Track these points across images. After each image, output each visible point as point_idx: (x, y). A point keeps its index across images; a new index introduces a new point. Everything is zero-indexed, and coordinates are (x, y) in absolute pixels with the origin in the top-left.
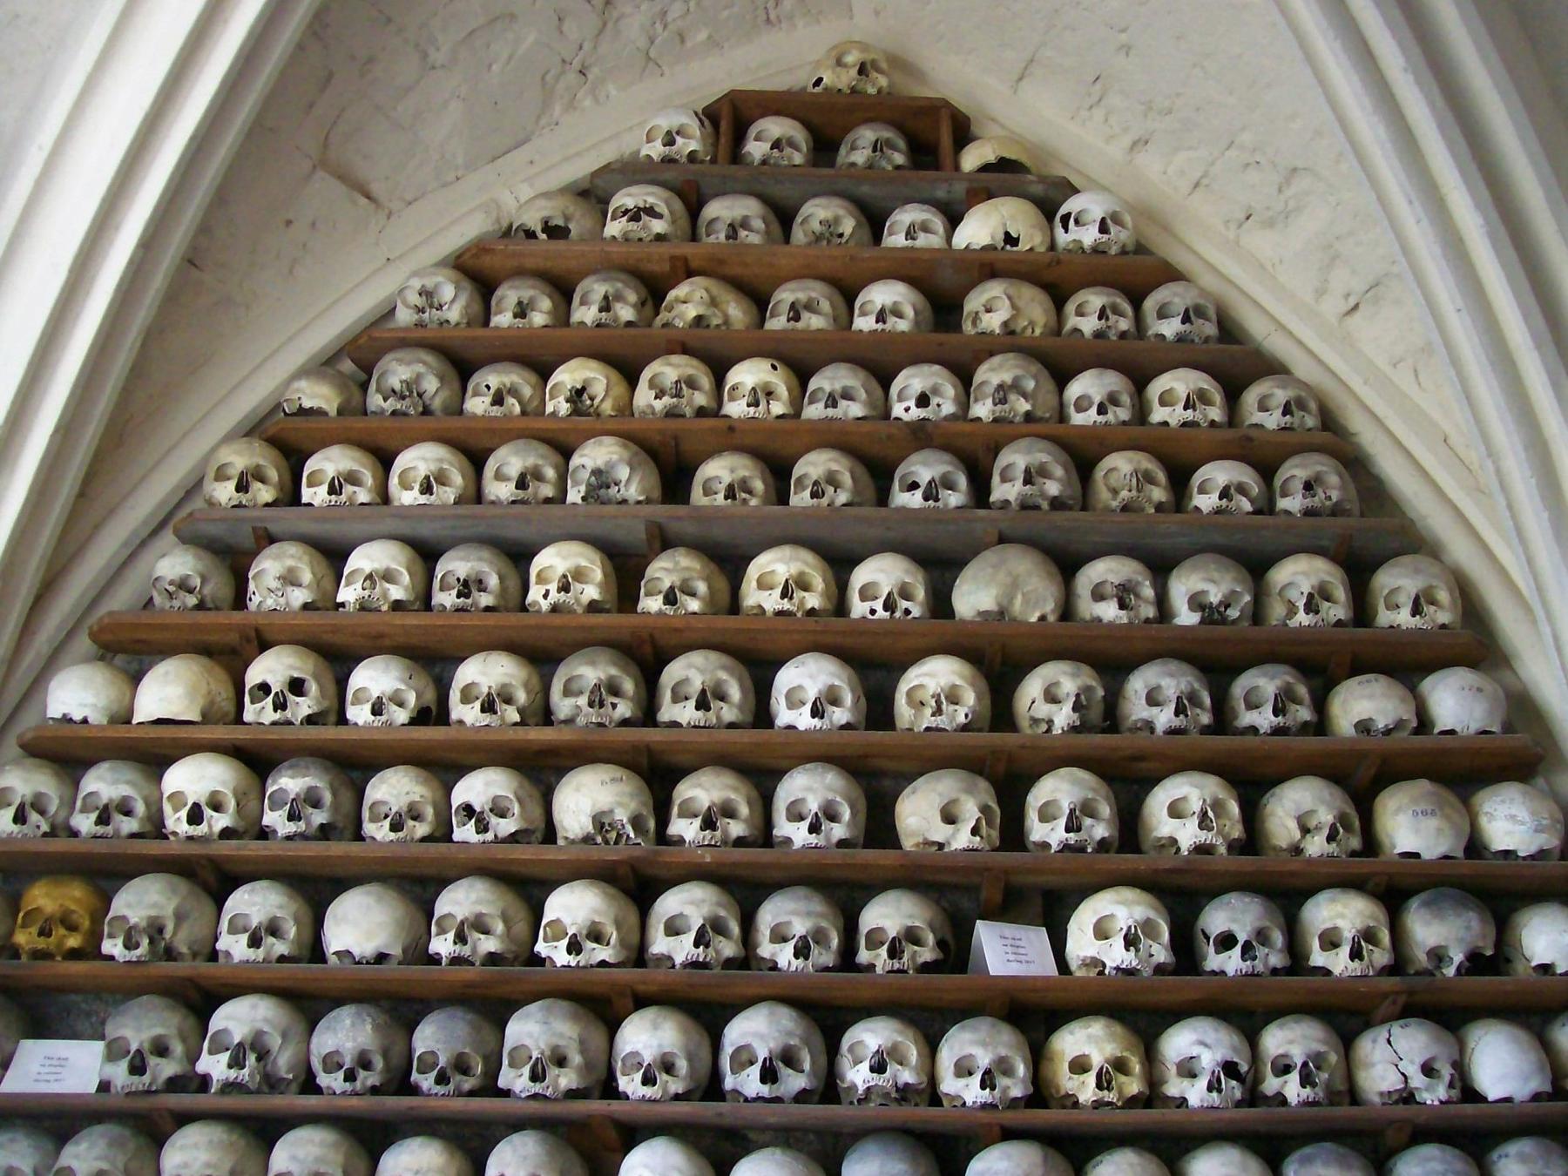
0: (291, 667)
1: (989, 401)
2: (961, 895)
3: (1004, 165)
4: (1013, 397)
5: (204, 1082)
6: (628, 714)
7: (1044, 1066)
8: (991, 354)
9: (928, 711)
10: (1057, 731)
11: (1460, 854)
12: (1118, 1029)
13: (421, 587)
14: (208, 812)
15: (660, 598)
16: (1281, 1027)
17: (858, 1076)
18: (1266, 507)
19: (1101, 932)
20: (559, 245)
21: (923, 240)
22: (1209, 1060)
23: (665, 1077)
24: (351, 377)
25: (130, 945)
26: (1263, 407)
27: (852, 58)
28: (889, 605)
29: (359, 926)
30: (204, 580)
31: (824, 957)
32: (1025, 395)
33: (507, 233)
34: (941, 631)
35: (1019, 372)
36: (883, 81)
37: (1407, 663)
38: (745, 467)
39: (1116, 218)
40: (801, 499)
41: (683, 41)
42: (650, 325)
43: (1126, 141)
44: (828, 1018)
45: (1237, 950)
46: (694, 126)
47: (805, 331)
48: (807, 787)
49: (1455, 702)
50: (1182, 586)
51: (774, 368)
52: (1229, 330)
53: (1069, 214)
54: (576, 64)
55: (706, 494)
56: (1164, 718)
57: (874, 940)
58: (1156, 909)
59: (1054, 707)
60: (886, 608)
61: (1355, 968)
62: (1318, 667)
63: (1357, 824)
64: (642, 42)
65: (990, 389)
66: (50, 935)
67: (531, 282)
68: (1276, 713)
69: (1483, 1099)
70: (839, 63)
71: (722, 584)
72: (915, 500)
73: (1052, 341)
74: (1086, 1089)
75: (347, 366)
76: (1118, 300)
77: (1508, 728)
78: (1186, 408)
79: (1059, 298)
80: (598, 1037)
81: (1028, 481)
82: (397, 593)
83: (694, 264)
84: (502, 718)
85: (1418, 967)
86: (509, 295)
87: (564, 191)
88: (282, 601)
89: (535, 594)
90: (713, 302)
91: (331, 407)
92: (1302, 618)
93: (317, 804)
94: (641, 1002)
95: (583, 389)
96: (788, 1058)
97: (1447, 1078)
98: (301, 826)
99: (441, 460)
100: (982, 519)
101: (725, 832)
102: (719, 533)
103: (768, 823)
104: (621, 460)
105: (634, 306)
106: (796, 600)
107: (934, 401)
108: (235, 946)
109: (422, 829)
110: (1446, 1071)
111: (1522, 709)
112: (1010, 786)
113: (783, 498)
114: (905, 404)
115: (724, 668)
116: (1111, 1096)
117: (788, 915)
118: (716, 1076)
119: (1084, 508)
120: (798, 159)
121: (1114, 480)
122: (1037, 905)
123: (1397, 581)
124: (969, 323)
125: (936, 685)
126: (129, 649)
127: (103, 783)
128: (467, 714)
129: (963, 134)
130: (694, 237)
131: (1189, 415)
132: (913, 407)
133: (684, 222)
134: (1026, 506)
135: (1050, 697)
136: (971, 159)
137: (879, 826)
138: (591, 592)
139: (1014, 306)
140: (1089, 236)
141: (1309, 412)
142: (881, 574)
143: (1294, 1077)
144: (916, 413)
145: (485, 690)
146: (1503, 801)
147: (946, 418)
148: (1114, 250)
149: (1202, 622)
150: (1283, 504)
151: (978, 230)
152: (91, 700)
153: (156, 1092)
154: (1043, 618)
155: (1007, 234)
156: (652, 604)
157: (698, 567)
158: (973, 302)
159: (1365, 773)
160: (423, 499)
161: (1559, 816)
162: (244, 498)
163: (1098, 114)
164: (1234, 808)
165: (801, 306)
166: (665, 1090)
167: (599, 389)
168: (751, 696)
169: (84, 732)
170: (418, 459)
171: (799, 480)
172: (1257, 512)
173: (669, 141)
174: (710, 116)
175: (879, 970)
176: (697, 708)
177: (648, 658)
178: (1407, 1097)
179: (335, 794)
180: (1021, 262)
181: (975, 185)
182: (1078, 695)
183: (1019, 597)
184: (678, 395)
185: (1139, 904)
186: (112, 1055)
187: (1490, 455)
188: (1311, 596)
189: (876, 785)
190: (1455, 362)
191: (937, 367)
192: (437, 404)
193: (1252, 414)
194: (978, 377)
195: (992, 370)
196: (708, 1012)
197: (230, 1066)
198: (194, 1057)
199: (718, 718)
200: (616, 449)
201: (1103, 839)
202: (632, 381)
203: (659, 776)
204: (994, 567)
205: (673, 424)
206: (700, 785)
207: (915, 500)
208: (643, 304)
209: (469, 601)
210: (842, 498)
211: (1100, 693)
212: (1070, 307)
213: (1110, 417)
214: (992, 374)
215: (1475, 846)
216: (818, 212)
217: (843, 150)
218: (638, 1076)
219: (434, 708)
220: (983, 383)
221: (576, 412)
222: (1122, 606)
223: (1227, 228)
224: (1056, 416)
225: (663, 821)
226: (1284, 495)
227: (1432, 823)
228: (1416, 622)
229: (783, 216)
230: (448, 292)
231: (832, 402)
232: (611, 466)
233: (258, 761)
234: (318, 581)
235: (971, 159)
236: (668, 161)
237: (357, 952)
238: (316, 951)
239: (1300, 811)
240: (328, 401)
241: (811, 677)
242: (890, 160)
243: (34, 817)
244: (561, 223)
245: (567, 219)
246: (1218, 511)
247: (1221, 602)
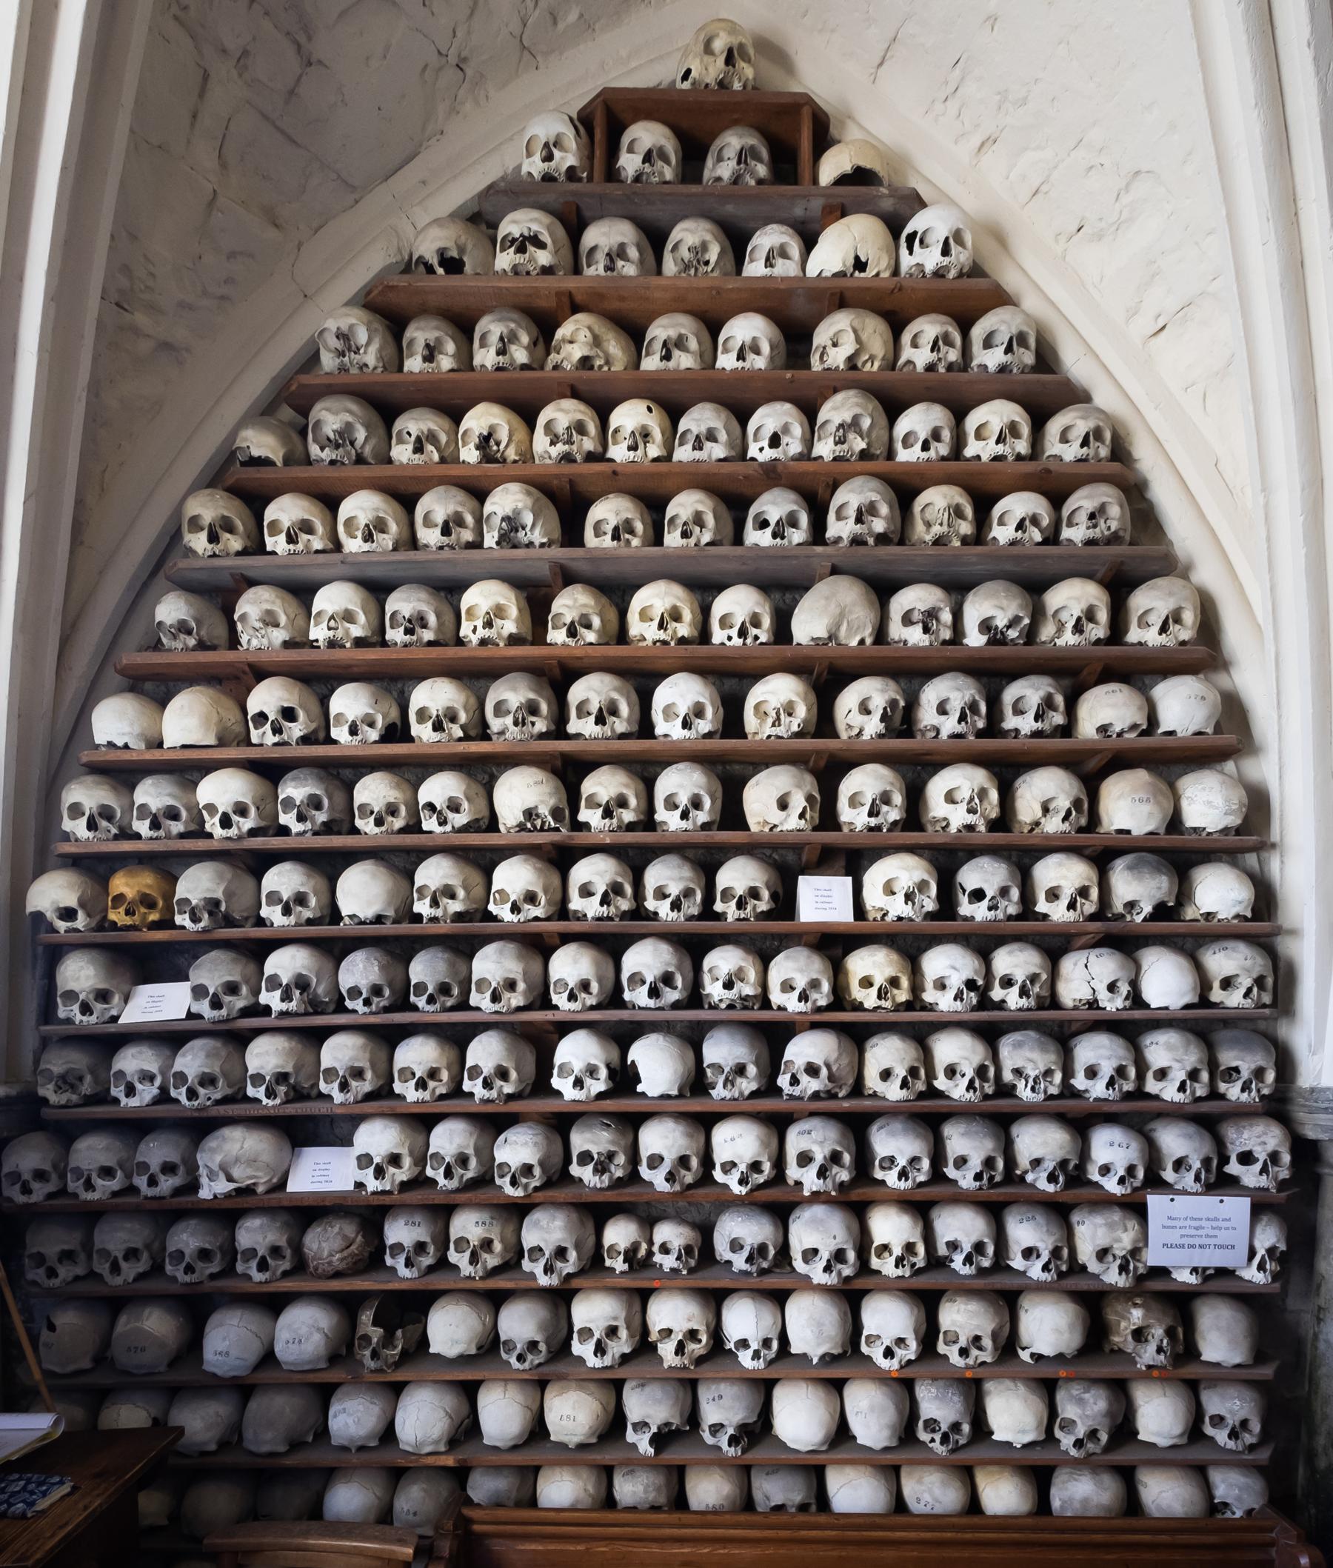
0: (281, 699)
1: (831, 440)
2: (787, 863)
3: (860, 177)
4: (851, 436)
5: (267, 1010)
6: (544, 730)
7: (841, 977)
8: (836, 391)
9: (770, 721)
10: (866, 736)
11: (1162, 831)
12: (895, 956)
13: (376, 622)
14: (235, 818)
15: (564, 630)
16: (1010, 953)
17: (714, 990)
18: (1052, 538)
19: (889, 890)
20: (455, 281)
22: (956, 981)
23: (583, 995)
24: (291, 424)
25: (195, 919)
26: (1064, 439)
27: (719, 45)
28: (743, 633)
29: (361, 892)
30: (198, 622)
31: (692, 907)
33: (407, 268)
34: (781, 652)
35: (858, 410)
36: (749, 72)
37: (1140, 672)
38: (627, 510)
39: (958, 236)
40: (673, 539)
41: (555, 22)
42: (542, 368)
43: (976, 140)
44: (693, 947)
45: (985, 903)
46: (569, 133)
47: (676, 371)
48: (679, 783)
49: (1182, 707)
51: (650, 410)
52: (1046, 359)
53: (915, 233)
54: (453, 59)
55: (597, 535)
56: (949, 725)
57: (727, 894)
58: (929, 873)
59: (866, 718)
60: (740, 636)
61: (1071, 916)
62: (1075, 677)
63: (1086, 806)
64: (515, 26)
65: (832, 428)
66: (134, 914)
67: (434, 323)
68: (1036, 720)
69: (1147, 1006)
70: (708, 50)
71: (612, 615)
72: (763, 538)
73: (889, 374)
74: (869, 999)
75: (287, 413)
76: (950, 329)
77: (1218, 729)
78: (998, 442)
79: (896, 324)
80: (536, 966)
81: (859, 520)
82: (356, 631)
83: (579, 298)
84: (450, 735)
85: (1116, 911)
86: (419, 334)
87: (453, 216)
88: (265, 641)
89: (465, 630)
90: (597, 341)
91: (278, 458)
92: (1069, 638)
93: (318, 807)
94: (566, 939)
95: (490, 435)
96: (667, 979)
97: (1125, 993)
98: (308, 825)
99: (377, 510)
100: (819, 555)
101: (620, 820)
102: (607, 570)
103: (651, 810)
104: (526, 507)
105: (527, 348)
106: (670, 631)
107: (785, 440)
108: (272, 914)
109: (398, 823)
110: (1124, 988)
111: (1233, 713)
112: (828, 774)
113: (658, 540)
114: (760, 445)
115: (615, 689)
116: (887, 1004)
117: (666, 876)
118: (618, 988)
119: (902, 542)
120: (669, 174)
121: (929, 515)
122: (841, 863)
123: (1151, 601)
124: (817, 356)
125: (776, 700)
126: (156, 687)
127: (152, 794)
128: (422, 732)
129: (823, 140)
130: (577, 270)
131: (1000, 449)
132: (766, 447)
133: (566, 252)
134: (857, 541)
135: (862, 707)
136: (832, 166)
137: (732, 814)
138: (509, 627)
139: (858, 340)
140: (930, 258)
141: (1103, 442)
142: (737, 603)
143: (1015, 990)
144: (769, 454)
145: (434, 714)
146: (1204, 789)
147: (794, 459)
148: (952, 274)
149: (989, 643)
150: (1067, 533)
151: (830, 255)
152: (127, 729)
153: (234, 1019)
154: (862, 642)
155: (857, 258)
156: (557, 636)
157: (592, 603)
158: (821, 336)
159: (1092, 764)
160: (366, 547)
161: (1246, 801)
162: (218, 549)
163: (953, 106)
164: (994, 795)
165: (671, 341)
166: (584, 1004)
167: (503, 435)
168: (637, 708)
169: (126, 756)
170: (361, 506)
171: (672, 520)
172: (1045, 542)
174: (584, 122)
175: (730, 919)
176: (597, 723)
177: (558, 678)
178: (1093, 1004)
179: (438, 616)
180: (868, 289)
181: (830, 201)
182: (885, 709)
183: (845, 624)
184: (569, 442)
186: (199, 992)
187: (1264, 490)
188: (1079, 619)
189: (730, 776)
190: (1256, 398)
191: (788, 406)
192: (367, 451)
193: (1053, 446)
194: (822, 416)
195: (835, 409)
196: (610, 944)
197: (283, 1000)
198: (257, 992)
199: (613, 730)
200: (521, 496)
202: (531, 425)
203: (570, 772)
204: (827, 598)
205: (567, 469)
206: (600, 784)
207: (763, 538)
208: (535, 344)
209: (414, 638)
210: (707, 537)
211: (902, 703)
212: (906, 337)
214: (836, 410)
215: (1175, 823)
216: (689, 234)
217: (710, 162)
218: (566, 995)
219: (399, 723)
220: (826, 422)
221: (488, 457)
222: (926, 630)
223: (1057, 241)
224: (885, 454)
225: (575, 809)
226: (1070, 524)
227: (1146, 808)
228: (1163, 640)
229: (655, 238)
230: (362, 336)
231: (698, 446)
232: (517, 512)
233: (270, 771)
234: (291, 621)
235: (832, 166)
236: (548, 178)
237: (362, 916)
238: (334, 915)
239: (1044, 794)
240: (273, 451)
242: (753, 173)
243: (104, 824)
244: (454, 254)
245: (462, 250)
246: (1013, 543)
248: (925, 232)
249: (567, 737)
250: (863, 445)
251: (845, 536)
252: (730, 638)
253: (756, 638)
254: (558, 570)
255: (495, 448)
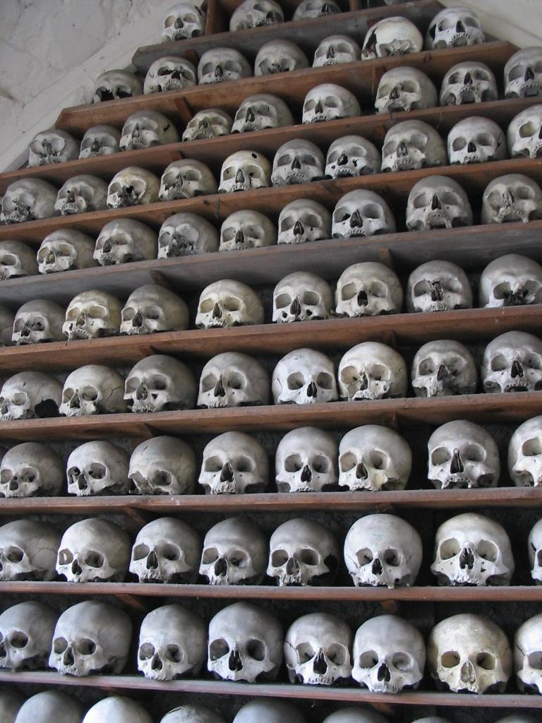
4: (411, 150)
12: (480, 628)
21: (338, 57)
23: (168, 663)
32: (422, 149)
38: (250, 219)
50: (490, 280)
51: (254, 156)
76: (480, 69)
83: (193, 102)
103: (272, 472)
106: (223, 318)
115: (235, 364)
121: (496, 202)
173: (180, 24)
185: (474, 529)
194: (332, 150)
201: (482, 476)
213: (478, 153)
236: (179, 38)
241: (307, 366)
247: (519, 291)
248: (441, 23)
249: (196, 407)
250: (423, 156)
251: (423, 220)
252: (285, 315)
253: (309, 313)
254: (160, 278)
255: (135, 197)
